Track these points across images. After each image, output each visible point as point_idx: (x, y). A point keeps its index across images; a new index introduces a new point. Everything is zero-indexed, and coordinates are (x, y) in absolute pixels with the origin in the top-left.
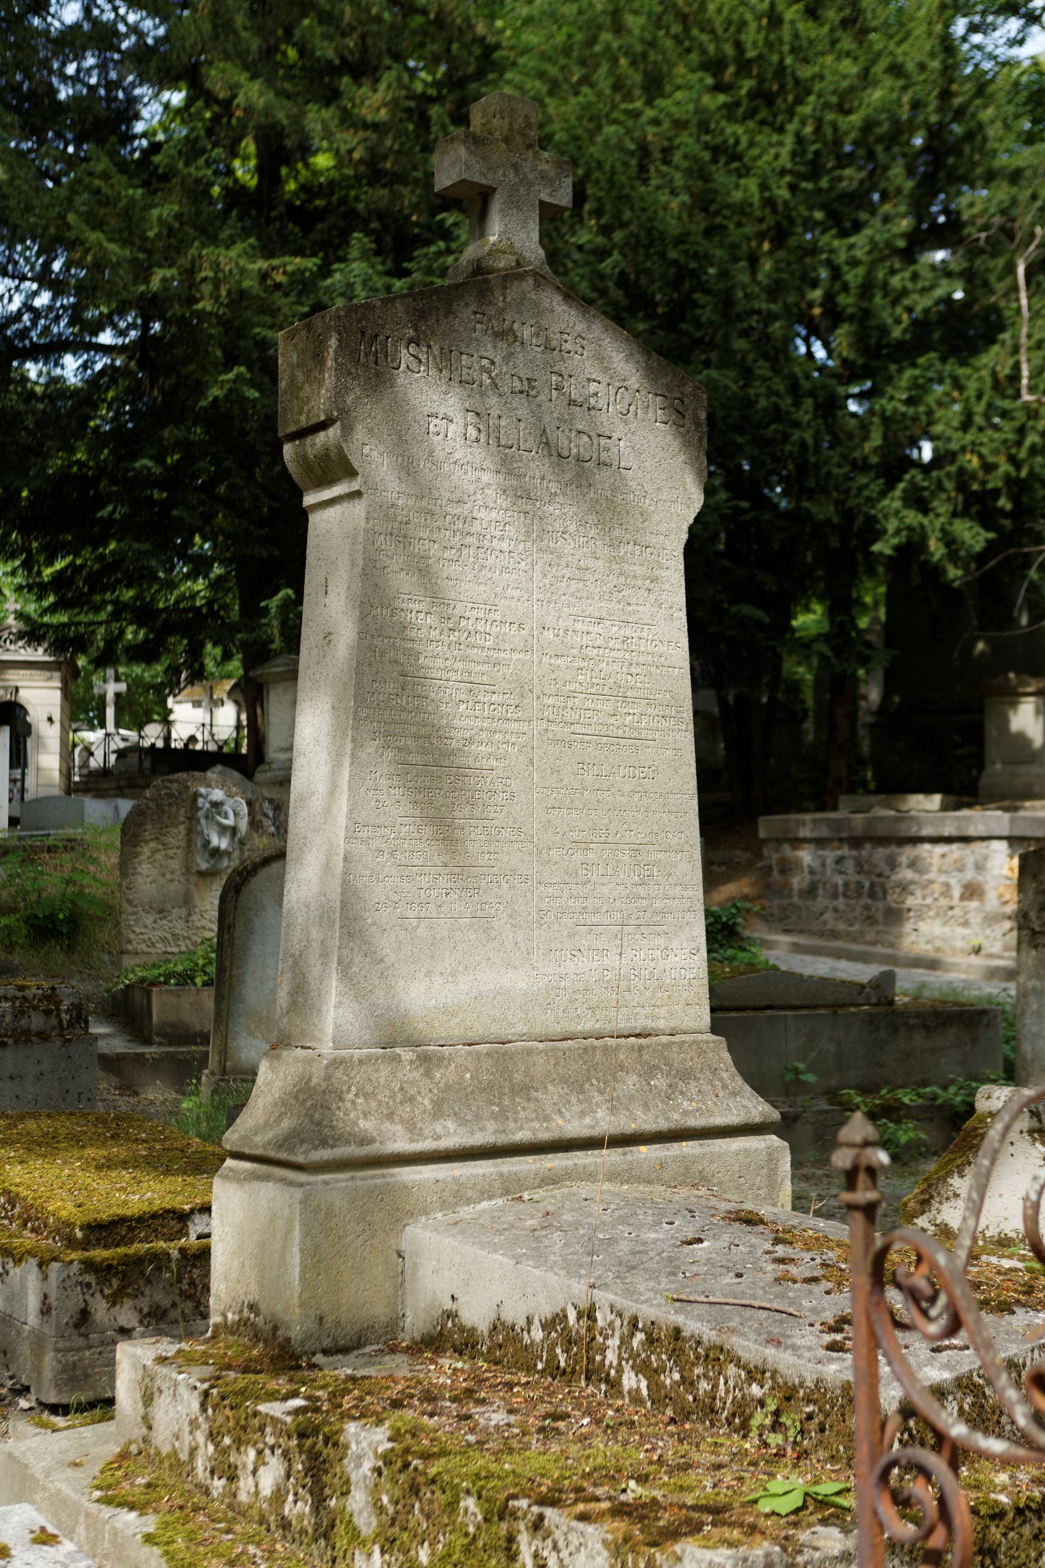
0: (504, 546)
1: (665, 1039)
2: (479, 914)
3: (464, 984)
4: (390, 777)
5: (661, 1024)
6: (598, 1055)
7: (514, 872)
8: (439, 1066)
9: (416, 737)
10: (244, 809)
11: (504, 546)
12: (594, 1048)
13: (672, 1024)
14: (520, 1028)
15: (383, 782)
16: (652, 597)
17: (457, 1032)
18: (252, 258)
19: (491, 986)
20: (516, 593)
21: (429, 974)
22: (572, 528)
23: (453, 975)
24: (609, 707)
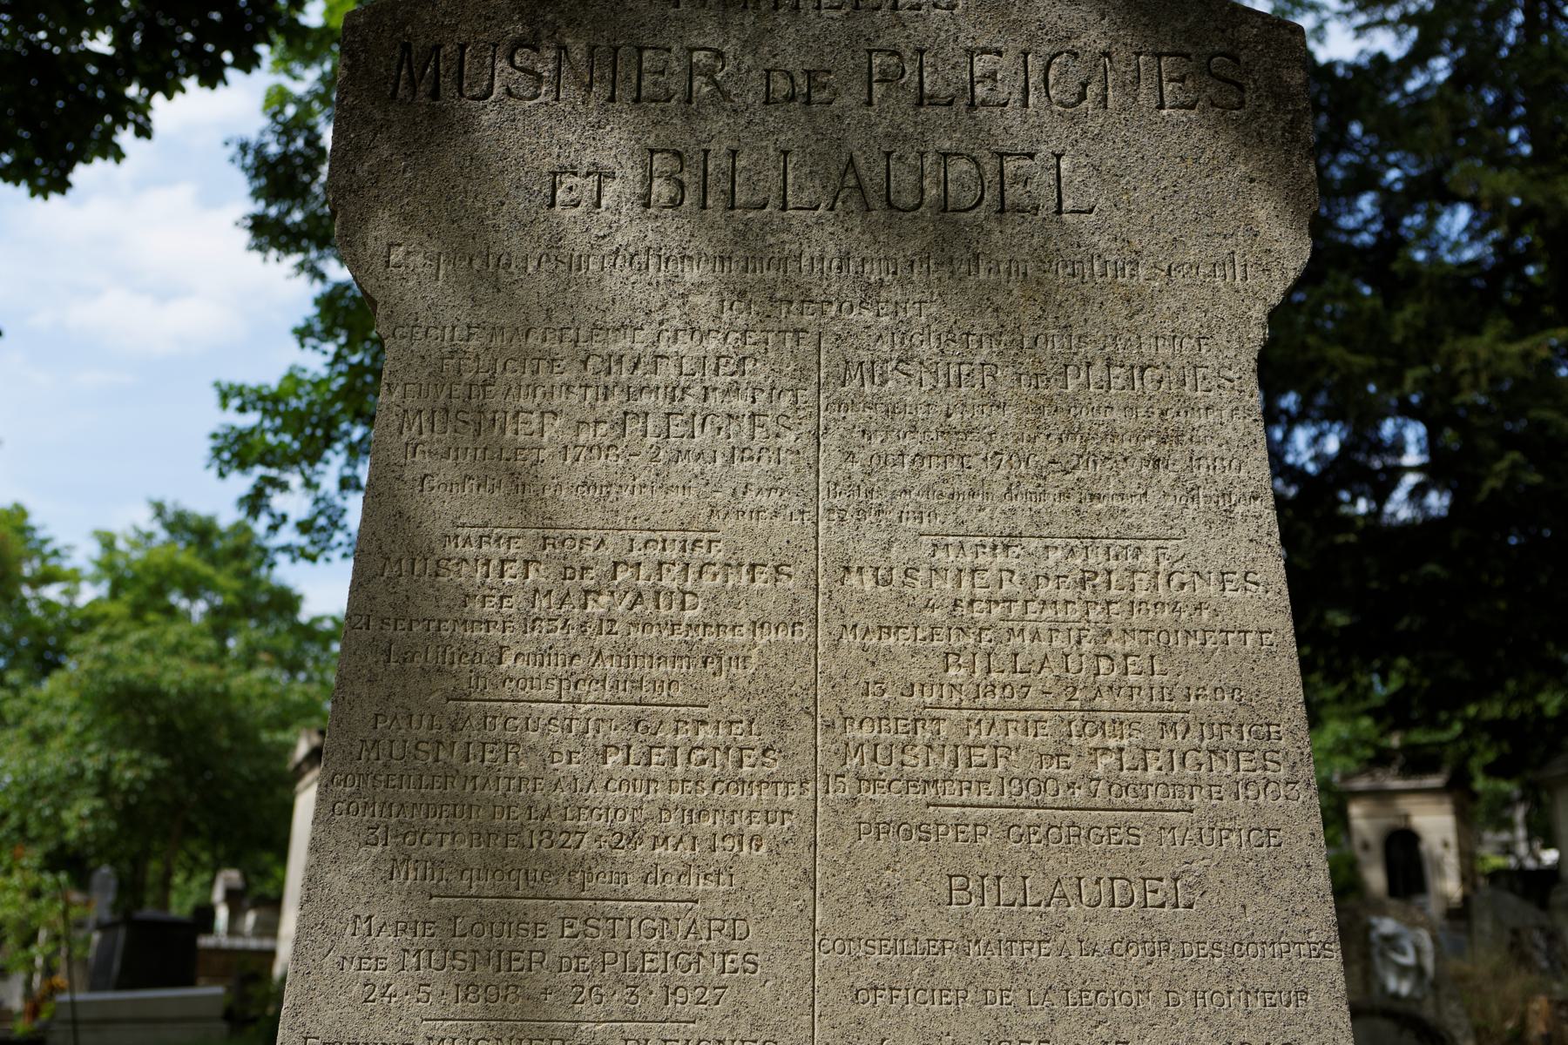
0: (740, 404)
4: (406, 926)
9: (483, 835)
10: (1427, 944)
11: (740, 404)
16: (1166, 477)
18: (1509, 339)
20: (769, 501)
22: (927, 350)
24: (1045, 740)
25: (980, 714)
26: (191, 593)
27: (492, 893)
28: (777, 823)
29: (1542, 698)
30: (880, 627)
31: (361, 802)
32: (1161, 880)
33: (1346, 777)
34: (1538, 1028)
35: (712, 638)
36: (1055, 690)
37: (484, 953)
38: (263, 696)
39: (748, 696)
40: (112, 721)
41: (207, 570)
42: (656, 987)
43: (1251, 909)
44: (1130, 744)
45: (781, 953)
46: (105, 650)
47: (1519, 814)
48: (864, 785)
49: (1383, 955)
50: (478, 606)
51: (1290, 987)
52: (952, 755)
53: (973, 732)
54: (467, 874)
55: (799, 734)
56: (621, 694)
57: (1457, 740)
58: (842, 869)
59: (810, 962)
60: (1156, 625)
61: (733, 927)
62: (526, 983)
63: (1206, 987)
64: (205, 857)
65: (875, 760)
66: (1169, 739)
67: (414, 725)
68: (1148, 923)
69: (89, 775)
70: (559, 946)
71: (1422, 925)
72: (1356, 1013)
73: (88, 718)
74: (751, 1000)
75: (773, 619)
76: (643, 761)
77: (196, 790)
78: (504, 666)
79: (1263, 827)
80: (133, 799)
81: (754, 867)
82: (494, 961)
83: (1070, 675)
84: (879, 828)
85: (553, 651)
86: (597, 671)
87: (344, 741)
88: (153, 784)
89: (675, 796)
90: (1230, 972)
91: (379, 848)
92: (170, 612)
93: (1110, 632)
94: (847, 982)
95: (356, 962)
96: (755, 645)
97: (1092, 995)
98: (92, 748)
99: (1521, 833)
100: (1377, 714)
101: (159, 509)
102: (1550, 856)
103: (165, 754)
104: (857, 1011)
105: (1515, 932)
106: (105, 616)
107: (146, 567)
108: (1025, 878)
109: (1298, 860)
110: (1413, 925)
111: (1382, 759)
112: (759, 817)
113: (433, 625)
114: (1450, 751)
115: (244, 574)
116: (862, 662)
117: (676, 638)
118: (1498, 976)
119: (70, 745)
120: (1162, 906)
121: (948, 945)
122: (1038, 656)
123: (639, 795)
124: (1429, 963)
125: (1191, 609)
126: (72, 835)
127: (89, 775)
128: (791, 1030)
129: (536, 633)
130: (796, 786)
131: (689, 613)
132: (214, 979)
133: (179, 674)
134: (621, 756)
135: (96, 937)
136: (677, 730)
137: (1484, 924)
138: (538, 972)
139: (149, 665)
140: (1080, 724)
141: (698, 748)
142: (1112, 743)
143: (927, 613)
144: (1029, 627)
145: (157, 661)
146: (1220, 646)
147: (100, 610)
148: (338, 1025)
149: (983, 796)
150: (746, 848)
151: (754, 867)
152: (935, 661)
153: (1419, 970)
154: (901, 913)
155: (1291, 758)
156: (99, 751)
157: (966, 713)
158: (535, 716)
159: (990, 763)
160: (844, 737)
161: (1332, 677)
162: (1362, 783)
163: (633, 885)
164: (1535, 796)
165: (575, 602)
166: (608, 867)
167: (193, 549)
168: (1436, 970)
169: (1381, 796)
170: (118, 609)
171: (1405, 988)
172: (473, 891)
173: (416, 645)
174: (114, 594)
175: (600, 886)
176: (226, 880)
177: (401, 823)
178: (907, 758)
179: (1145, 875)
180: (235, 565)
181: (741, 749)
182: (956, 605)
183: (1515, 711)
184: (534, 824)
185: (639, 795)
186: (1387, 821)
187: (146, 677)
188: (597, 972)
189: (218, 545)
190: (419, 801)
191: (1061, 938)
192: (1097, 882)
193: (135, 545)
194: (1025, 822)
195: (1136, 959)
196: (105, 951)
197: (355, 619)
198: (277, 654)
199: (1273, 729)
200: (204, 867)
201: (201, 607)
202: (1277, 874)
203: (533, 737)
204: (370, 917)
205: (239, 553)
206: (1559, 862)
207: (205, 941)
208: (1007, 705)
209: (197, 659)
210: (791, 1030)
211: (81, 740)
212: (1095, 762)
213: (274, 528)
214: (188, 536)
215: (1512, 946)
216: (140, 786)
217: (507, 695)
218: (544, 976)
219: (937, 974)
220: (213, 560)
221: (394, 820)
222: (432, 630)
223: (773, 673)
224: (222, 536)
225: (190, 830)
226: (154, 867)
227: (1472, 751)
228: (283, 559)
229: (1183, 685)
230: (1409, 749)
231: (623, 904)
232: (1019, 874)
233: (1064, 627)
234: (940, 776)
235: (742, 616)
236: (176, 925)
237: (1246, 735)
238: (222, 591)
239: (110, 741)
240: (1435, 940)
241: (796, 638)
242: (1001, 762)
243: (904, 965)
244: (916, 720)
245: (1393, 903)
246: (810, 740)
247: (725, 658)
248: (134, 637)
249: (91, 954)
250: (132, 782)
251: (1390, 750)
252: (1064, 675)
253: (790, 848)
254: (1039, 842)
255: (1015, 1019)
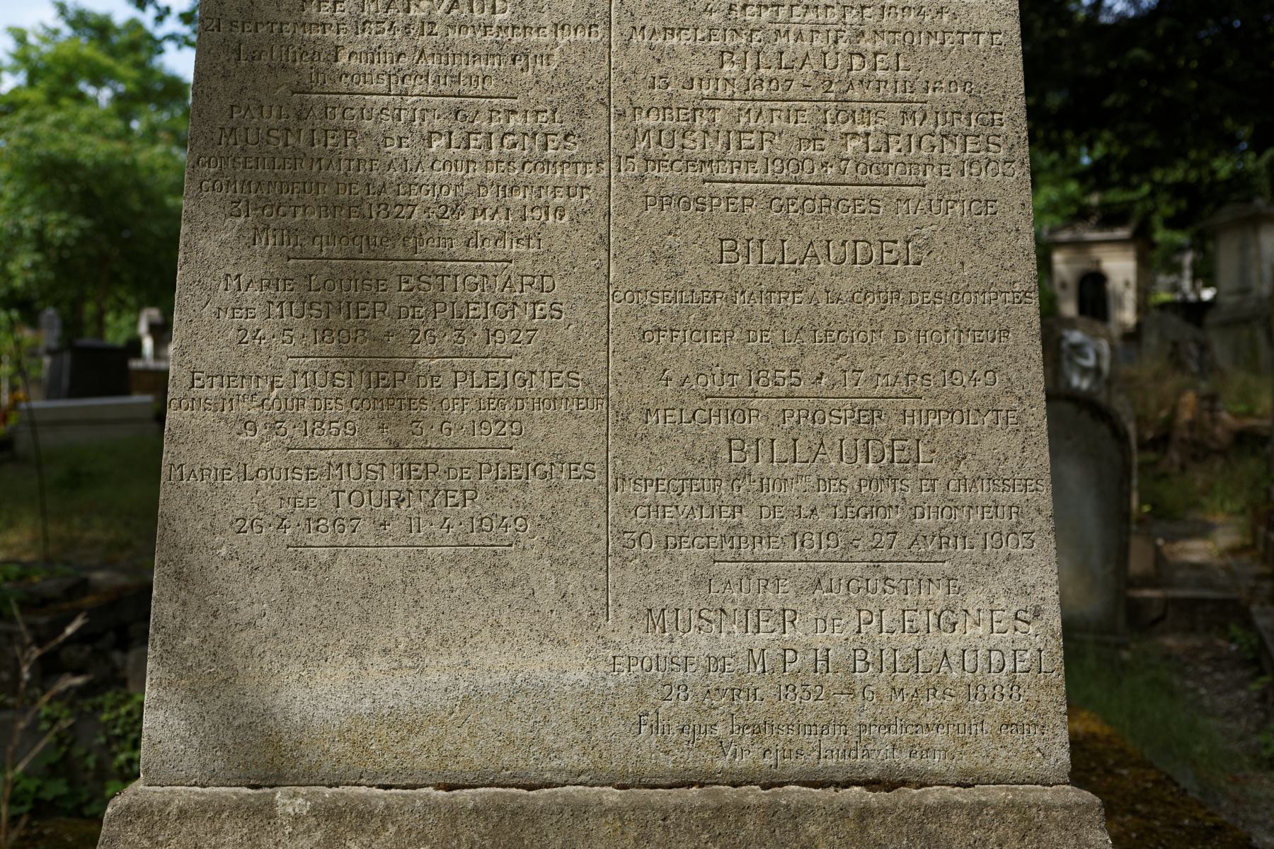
1: (933, 795)
2: (474, 537)
3: (439, 675)
4: (270, 283)
5: (936, 763)
6: (751, 824)
7: (560, 457)
8: (359, 830)
9: (330, 207)
12: (742, 809)
13: (965, 763)
14: (572, 759)
15: (253, 294)
17: (421, 761)
19: (504, 677)
21: (356, 652)
23: (411, 653)
24: (804, 126)
25: (750, 105)
26: (98, 82)
27: (339, 255)
28: (577, 197)
29: (1217, 163)
30: (665, 29)
31: (224, 180)
32: (895, 242)
33: (1053, 231)
34: (1186, 415)
35: (520, 39)
36: (814, 84)
37: (336, 304)
38: (165, 167)
39: (551, 89)
40: (41, 189)
41: (107, 61)
42: (479, 331)
43: (968, 265)
44: (876, 130)
45: (581, 303)
46: (28, 128)
47: (1188, 259)
48: (651, 165)
49: (1070, 359)
50: (314, 10)
51: (996, 327)
52: (725, 139)
53: (743, 120)
54: (318, 240)
55: (595, 122)
56: (442, 87)
57: (1143, 199)
58: (632, 234)
59: (605, 310)
60: (902, 27)
61: (541, 282)
62: (372, 327)
63: (927, 327)
64: (131, 301)
65: (660, 143)
66: (908, 126)
67: (265, 115)
68: (883, 277)
69: (27, 233)
70: (398, 298)
71: (1103, 336)
72: (1051, 397)
73: (20, 186)
74: (557, 340)
75: (573, 22)
76: (463, 145)
77: (114, 246)
78: (340, 63)
79: (983, 199)
80: (66, 254)
81: (558, 233)
82: (344, 310)
83: (827, 71)
84: (663, 200)
85: (382, 50)
86: (421, 67)
87: (205, 129)
88: (83, 240)
89: (491, 175)
90: (948, 315)
91: (242, 219)
92: (80, 98)
93: (863, 33)
94: (636, 325)
95: (230, 312)
96: (557, 45)
97: (835, 334)
98: (26, 210)
99: (1187, 273)
100: (1082, 176)
101: (62, 9)
102: (1207, 294)
103: (88, 216)
104: (644, 348)
105: (1175, 344)
106: (25, 102)
107: (57, 59)
108: (783, 241)
109: (1010, 226)
110: (1096, 336)
111: (1082, 215)
112: (562, 191)
113: (276, 27)
114: (1139, 208)
115: (140, 65)
116: (650, 60)
117: (489, 38)
118: (1158, 378)
119: (7, 210)
120: (896, 263)
121: (719, 295)
122: (800, 54)
123: (460, 174)
124: (1105, 365)
125: (933, 13)
126: (18, 283)
127: (27, 233)
128: (590, 363)
129: (366, 34)
130: (593, 165)
131: (499, 17)
132: (145, 391)
133: (93, 149)
134: (443, 141)
135: (47, 361)
136: (491, 119)
137: (1152, 339)
138: (381, 319)
139: (67, 141)
140: (834, 112)
141: (509, 133)
142: (860, 129)
143: (706, 16)
144: (793, 28)
145: (73, 138)
146: (956, 45)
147: (21, 96)
148: (218, 362)
149: (750, 174)
150: (551, 217)
151: (558, 233)
152: (712, 59)
153: (1097, 371)
154: (680, 270)
155: (1010, 141)
156: (32, 214)
157: (737, 104)
158: (369, 106)
159: (757, 145)
160: (633, 124)
161: (1049, 146)
162: (1065, 236)
163: (458, 248)
164: (1201, 242)
165: (400, 7)
166: (436, 234)
167: (95, 44)
168: (1111, 371)
169: (1080, 246)
170: (36, 95)
171: (1085, 384)
172: (324, 254)
173: (262, 44)
174: (32, 81)
175: (430, 249)
176: (149, 316)
177: (259, 198)
178: (687, 142)
179: (883, 238)
180: (131, 57)
181: (546, 135)
182: (731, 9)
183: (1193, 175)
184: (372, 198)
185: (460, 174)
186: (1082, 266)
187: (63, 150)
188: (430, 319)
189: (116, 39)
190: (273, 179)
191: (811, 290)
192: (843, 244)
193: (45, 40)
194: (785, 195)
195: (872, 305)
196: (55, 371)
197: (207, 22)
198: (174, 133)
199: (996, 117)
200: (131, 309)
201: (105, 94)
202: (992, 237)
203: (368, 124)
204: (238, 276)
205: (134, 47)
206: (1215, 297)
207: (135, 364)
208: (773, 97)
209: (107, 137)
210: (590, 363)
211: (16, 205)
212: (845, 145)
213: (159, 19)
214: (88, 32)
215: (1172, 355)
216: (70, 242)
217: (344, 88)
218: (386, 323)
219: (709, 319)
220: (113, 53)
221: (253, 195)
222: (276, 31)
223: (573, 69)
224: (118, 31)
225: (115, 278)
226: (90, 308)
227: (1155, 210)
228: (170, 46)
229: (922, 79)
230: (1104, 206)
231: (449, 264)
232: (778, 238)
233: (824, 28)
234: (715, 157)
235: (545, 19)
236: (113, 351)
237: (973, 122)
238: (122, 79)
239: (41, 205)
240: (1112, 347)
241: (593, 39)
242: (766, 145)
243: (683, 311)
244: (695, 110)
245: (1083, 320)
246: (604, 127)
247: (531, 56)
248: (52, 118)
249: (44, 374)
250: (64, 238)
251: (1088, 206)
252: (822, 71)
253: (589, 217)
254: (796, 211)
255: (772, 353)
